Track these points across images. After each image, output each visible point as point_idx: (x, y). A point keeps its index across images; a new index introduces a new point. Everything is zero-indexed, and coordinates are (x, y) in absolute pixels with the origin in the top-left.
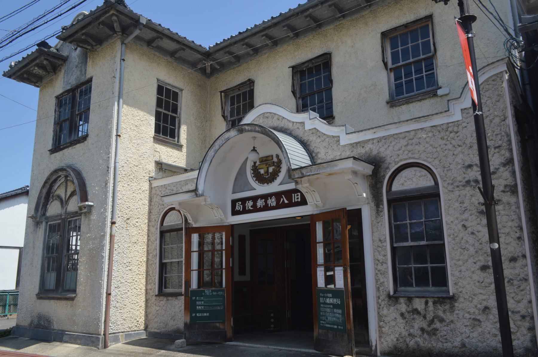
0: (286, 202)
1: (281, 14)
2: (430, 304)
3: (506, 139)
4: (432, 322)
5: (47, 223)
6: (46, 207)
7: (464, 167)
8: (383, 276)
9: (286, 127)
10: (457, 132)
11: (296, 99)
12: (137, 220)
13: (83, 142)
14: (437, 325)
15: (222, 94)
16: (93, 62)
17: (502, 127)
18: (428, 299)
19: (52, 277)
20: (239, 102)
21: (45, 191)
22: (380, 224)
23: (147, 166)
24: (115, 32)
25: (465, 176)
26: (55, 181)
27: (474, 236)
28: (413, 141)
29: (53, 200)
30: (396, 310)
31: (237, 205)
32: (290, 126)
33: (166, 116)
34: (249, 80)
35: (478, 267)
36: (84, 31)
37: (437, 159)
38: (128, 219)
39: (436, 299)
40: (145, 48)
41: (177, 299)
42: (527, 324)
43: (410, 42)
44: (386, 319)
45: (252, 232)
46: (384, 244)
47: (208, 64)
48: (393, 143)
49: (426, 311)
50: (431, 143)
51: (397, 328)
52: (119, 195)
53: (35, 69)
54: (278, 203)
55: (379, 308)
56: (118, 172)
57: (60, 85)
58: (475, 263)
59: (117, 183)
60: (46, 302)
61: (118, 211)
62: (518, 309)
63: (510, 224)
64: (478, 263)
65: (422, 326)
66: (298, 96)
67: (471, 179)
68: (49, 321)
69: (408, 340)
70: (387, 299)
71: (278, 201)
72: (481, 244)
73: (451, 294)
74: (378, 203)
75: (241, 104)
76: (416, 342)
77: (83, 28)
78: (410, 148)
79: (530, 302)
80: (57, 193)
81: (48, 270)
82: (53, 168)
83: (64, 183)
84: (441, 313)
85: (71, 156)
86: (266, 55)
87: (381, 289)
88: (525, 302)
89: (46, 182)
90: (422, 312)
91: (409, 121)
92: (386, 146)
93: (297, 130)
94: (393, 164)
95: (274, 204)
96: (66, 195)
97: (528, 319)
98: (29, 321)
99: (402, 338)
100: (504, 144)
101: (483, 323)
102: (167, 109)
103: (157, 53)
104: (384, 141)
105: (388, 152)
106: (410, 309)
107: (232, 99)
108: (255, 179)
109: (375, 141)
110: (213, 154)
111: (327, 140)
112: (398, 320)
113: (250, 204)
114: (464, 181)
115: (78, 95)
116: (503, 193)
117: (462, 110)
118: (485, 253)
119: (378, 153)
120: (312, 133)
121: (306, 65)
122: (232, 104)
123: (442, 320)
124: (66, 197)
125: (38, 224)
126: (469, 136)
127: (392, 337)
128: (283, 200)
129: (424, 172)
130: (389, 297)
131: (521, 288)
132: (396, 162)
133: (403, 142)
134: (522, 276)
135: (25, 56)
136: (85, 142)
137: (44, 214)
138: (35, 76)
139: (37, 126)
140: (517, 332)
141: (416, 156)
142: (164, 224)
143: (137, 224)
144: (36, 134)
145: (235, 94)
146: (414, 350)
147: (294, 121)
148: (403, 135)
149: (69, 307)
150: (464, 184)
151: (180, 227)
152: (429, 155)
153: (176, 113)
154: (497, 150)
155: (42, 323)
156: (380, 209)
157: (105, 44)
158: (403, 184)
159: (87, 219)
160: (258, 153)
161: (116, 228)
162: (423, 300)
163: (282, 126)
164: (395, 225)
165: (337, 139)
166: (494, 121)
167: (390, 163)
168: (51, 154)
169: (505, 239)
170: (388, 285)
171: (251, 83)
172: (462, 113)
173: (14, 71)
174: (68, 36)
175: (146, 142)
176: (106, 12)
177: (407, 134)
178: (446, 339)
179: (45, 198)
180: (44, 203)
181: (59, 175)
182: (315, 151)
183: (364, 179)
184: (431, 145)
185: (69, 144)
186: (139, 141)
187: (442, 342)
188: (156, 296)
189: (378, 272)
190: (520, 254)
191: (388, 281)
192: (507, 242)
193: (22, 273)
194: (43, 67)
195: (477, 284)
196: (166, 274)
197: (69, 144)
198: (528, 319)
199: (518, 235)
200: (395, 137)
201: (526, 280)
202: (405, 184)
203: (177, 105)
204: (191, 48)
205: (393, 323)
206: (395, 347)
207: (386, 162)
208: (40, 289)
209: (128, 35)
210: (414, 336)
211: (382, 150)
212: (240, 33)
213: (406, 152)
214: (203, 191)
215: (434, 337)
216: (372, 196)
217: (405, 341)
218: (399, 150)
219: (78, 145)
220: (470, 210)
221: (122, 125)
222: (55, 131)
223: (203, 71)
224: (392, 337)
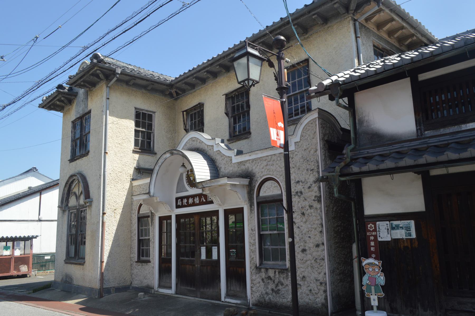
0: (204, 201)
2: (277, 273)
3: (316, 165)
4: (277, 285)
9: (204, 148)
14: (280, 287)
15: (185, 113)
19: (73, 248)
20: (195, 119)
21: (66, 189)
24: (101, 80)
25: (296, 188)
26: (72, 182)
34: (199, 103)
36: (82, 80)
40: (125, 86)
42: (323, 288)
43: (296, 77)
47: (173, 91)
48: (260, 164)
51: (260, 288)
52: (107, 194)
53: (58, 101)
54: (200, 201)
56: (107, 178)
57: (74, 112)
59: (106, 186)
62: (319, 278)
63: (317, 222)
64: (301, 247)
66: (230, 115)
67: (299, 191)
68: (71, 279)
69: (265, 296)
71: (200, 199)
74: (251, 205)
76: (269, 298)
77: (81, 78)
78: (268, 167)
79: (325, 274)
80: (74, 190)
81: (71, 244)
82: (72, 172)
85: (82, 165)
86: (211, 84)
88: (322, 273)
89: (66, 183)
90: (273, 278)
92: (256, 166)
94: (259, 178)
95: (198, 202)
97: (323, 285)
98: (61, 277)
103: (134, 89)
107: (191, 115)
109: (250, 162)
110: (158, 168)
111: (226, 159)
113: (185, 201)
115: (84, 121)
117: (295, 143)
121: (234, 93)
122: (191, 120)
123: (282, 284)
125: (64, 211)
127: (258, 294)
129: (277, 184)
130: (256, 267)
131: (321, 265)
132: (261, 177)
133: (265, 163)
134: (322, 257)
135: (50, 95)
137: (67, 205)
138: (58, 106)
141: (271, 173)
145: (193, 112)
146: (268, 303)
153: (151, 130)
154: (312, 172)
157: (97, 87)
158: (265, 192)
162: (273, 271)
164: (262, 220)
171: (200, 106)
172: (295, 145)
173: (46, 103)
176: (92, 69)
177: (267, 158)
178: (284, 296)
183: (243, 187)
184: (279, 166)
188: (136, 262)
189: (252, 251)
190: (321, 243)
194: (62, 101)
198: (323, 285)
199: (320, 229)
201: (323, 259)
202: (267, 192)
204: (158, 83)
205: (258, 285)
206: (259, 301)
208: (66, 256)
209: (111, 80)
211: (254, 168)
212: (190, 71)
213: (266, 170)
217: (264, 297)
218: (263, 168)
219: (84, 158)
221: (108, 144)
222: (72, 146)
223: (171, 95)
224: (258, 294)
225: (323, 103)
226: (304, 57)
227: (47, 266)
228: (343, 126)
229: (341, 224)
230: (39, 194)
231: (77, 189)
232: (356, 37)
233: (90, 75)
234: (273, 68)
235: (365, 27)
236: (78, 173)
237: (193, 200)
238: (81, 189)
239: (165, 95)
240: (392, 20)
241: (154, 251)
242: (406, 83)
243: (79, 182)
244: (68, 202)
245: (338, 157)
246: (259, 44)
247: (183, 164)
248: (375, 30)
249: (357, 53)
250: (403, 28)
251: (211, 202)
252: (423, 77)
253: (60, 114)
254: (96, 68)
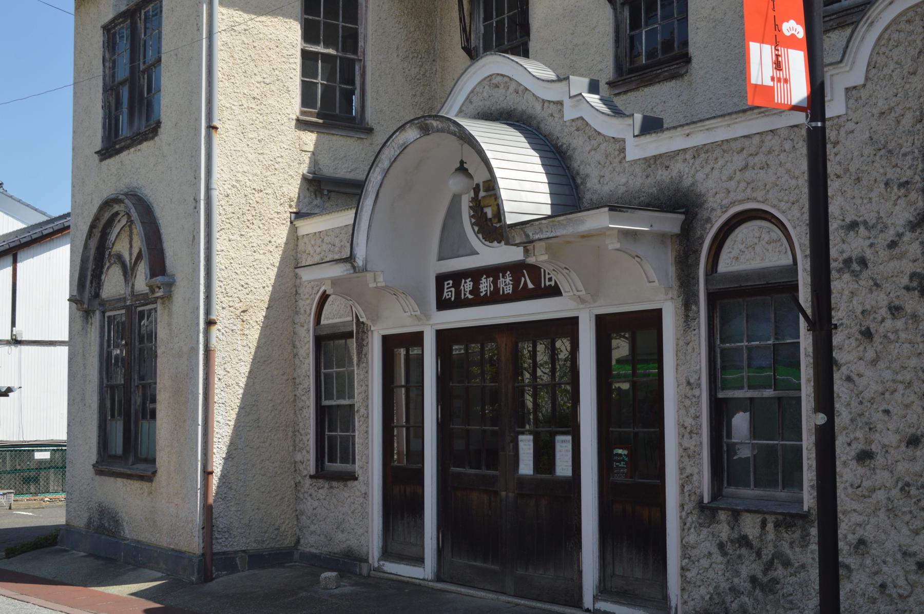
0: (530, 286)
2: (770, 526)
4: (769, 566)
5: (103, 313)
6: (100, 279)
7: (842, 227)
8: (691, 463)
11: (615, 9)
13: (153, 138)
14: (779, 572)
17: (917, 137)
18: (767, 516)
21: (93, 244)
22: (690, 347)
23: (285, 190)
25: (845, 247)
26: (110, 223)
27: (851, 386)
28: (757, 159)
29: (111, 265)
30: (711, 536)
31: (446, 287)
32: (537, 109)
35: (853, 453)
37: (796, 206)
38: (244, 312)
39: (781, 518)
41: (345, 486)
44: (694, 553)
46: (696, 392)
48: (721, 162)
49: (762, 540)
50: (788, 165)
51: (711, 575)
55: (683, 530)
58: (849, 444)
60: (110, 481)
61: (220, 296)
62: (915, 549)
64: (854, 446)
65: (753, 572)
67: (854, 255)
69: (728, 599)
70: (696, 512)
72: (861, 403)
73: (806, 508)
75: (505, 16)
78: (749, 175)
81: (113, 416)
83: (127, 229)
84: (786, 548)
85: (138, 167)
87: (686, 489)
89: (93, 226)
90: (756, 543)
91: (749, 113)
92: (707, 169)
93: (550, 119)
94: (719, 212)
95: (509, 290)
96: (131, 254)
99: (719, 594)
100: (917, 178)
101: (854, 573)
104: (703, 155)
105: (710, 183)
106: (735, 535)
108: (476, 229)
109: (688, 156)
110: (380, 178)
111: (603, 147)
112: (714, 556)
114: (841, 259)
115: (141, 25)
116: (905, 292)
117: (847, 90)
118: (867, 424)
119: (693, 184)
120: (578, 130)
123: (787, 563)
124: (131, 259)
125: (88, 314)
126: (856, 154)
128: (525, 281)
133: (738, 161)
136: (157, 139)
137: (97, 295)
139: (75, 93)
140: (909, 596)
141: (760, 195)
142: (322, 323)
144: (75, 111)
147: (546, 99)
148: (737, 145)
149: (146, 494)
150: (841, 265)
151: (349, 329)
152: (782, 193)
153: (355, 51)
154: (903, 191)
155: (106, 525)
156: (691, 314)
159: (166, 312)
161: (218, 334)
162: (758, 518)
163: (524, 107)
165: (620, 144)
166: (903, 122)
167: (713, 210)
168: (101, 160)
169: (903, 395)
170: (700, 482)
172: (847, 99)
177: (747, 143)
178: (791, 602)
179: (95, 259)
180: (93, 271)
181: (115, 210)
182: (581, 172)
184: (788, 171)
185: (129, 141)
186: (263, 134)
187: (784, 608)
188: (311, 477)
189: (686, 453)
191: (700, 473)
192: (906, 402)
195: (850, 490)
196: (723, 341)
197: (129, 141)
200: (725, 147)
203: (357, 29)
205: (705, 563)
207: (706, 206)
210: (739, 591)
211: (700, 176)
213: (743, 184)
214: (366, 260)
215: (771, 597)
216: (678, 284)
217: (724, 602)
218: (731, 179)
219: (145, 144)
220: (847, 327)
221: (220, 100)
222: (106, 107)
224: (703, 591)
230: (9, 259)
231: (126, 245)
236: (126, 194)
237: (495, 283)
238: (138, 244)
241: (366, 446)
243: (130, 222)
251: (554, 291)
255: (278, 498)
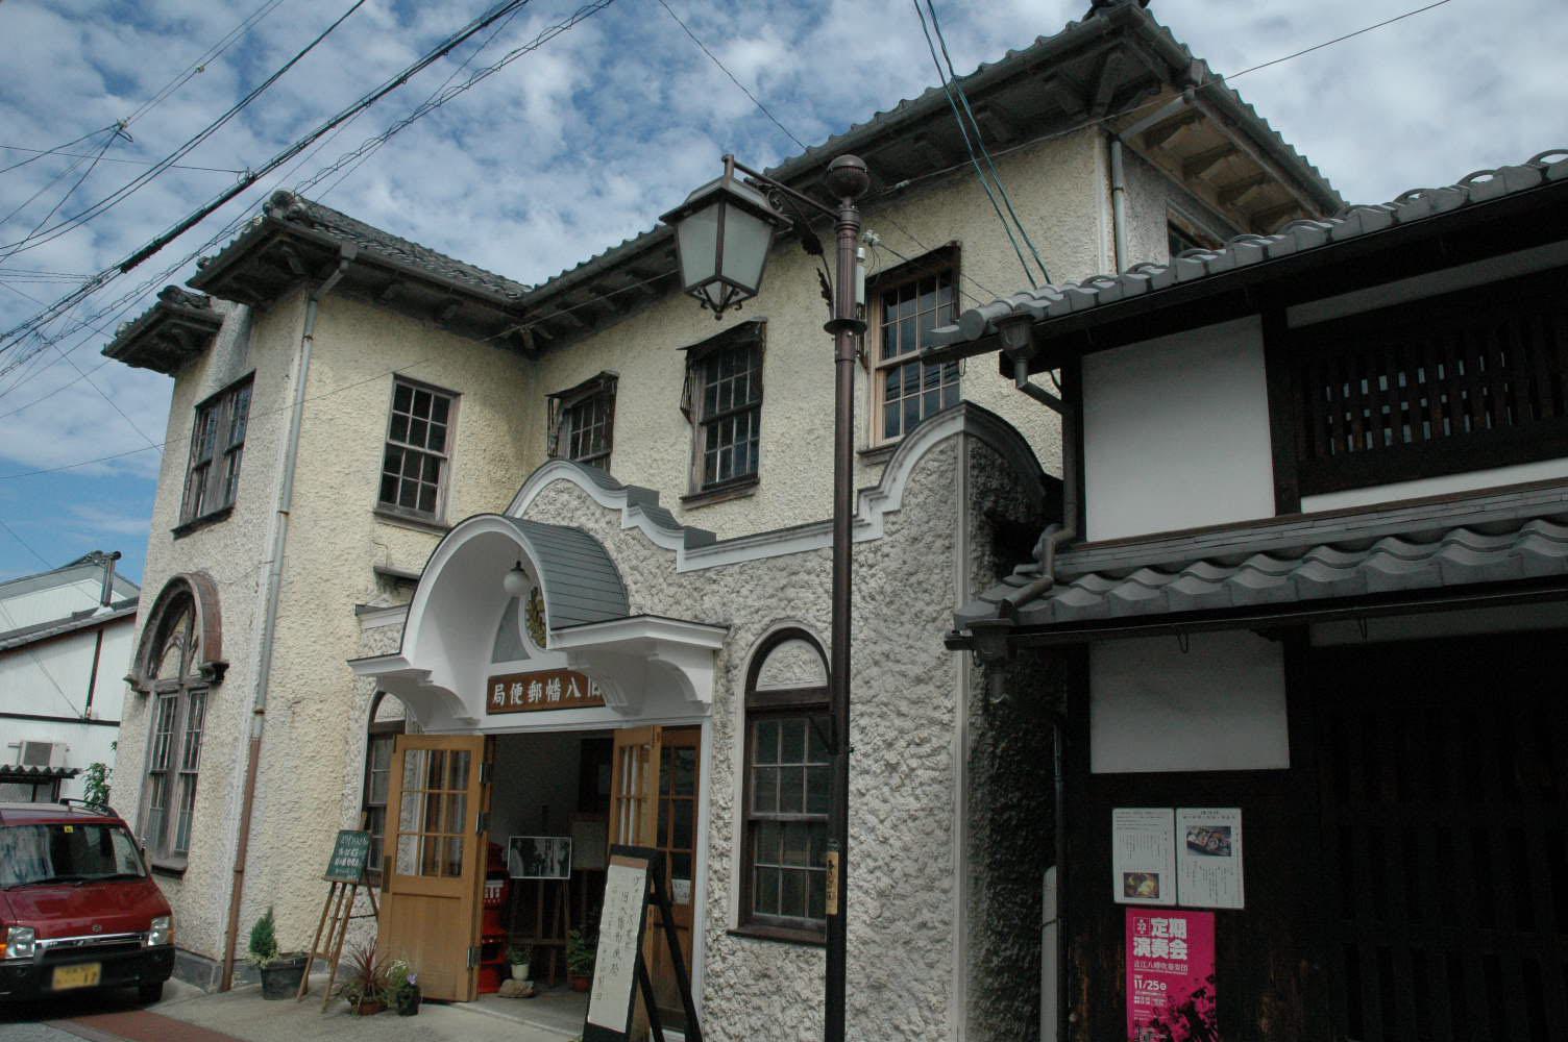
1: (625, 242)
10: (871, 567)
12: (319, 706)
16: (260, 334)
24: (297, 277)
33: (414, 457)
45: (584, 742)
47: (524, 329)
53: (163, 341)
71: (564, 690)
95: (556, 697)
102: (418, 439)
143: (318, 714)
153: (440, 448)
160: (527, 576)
168: (176, 539)
174: (219, 277)
175: (1013, 263)
177: (788, 560)
193: (259, 791)
203: (396, 408)
223: (516, 344)
225: (982, 380)
226: (941, 240)
227: (61, 893)
228: (1046, 471)
229: (1020, 800)
230: (93, 639)
232: (1113, 190)
233: (260, 259)
234: (817, 257)
235: (1143, 162)
237: (544, 690)
239: (499, 343)
240: (1231, 149)
242: (1248, 331)
244: (157, 667)
245: (1019, 568)
246: (805, 191)
247: (519, 563)
248: (1176, 178)
249: (1112, 235)
250: (1263, 179)
251: (598, 702)
252: (1303, 314)
253: (166, 382)
254: (278, 239)
255: (313, 903)
